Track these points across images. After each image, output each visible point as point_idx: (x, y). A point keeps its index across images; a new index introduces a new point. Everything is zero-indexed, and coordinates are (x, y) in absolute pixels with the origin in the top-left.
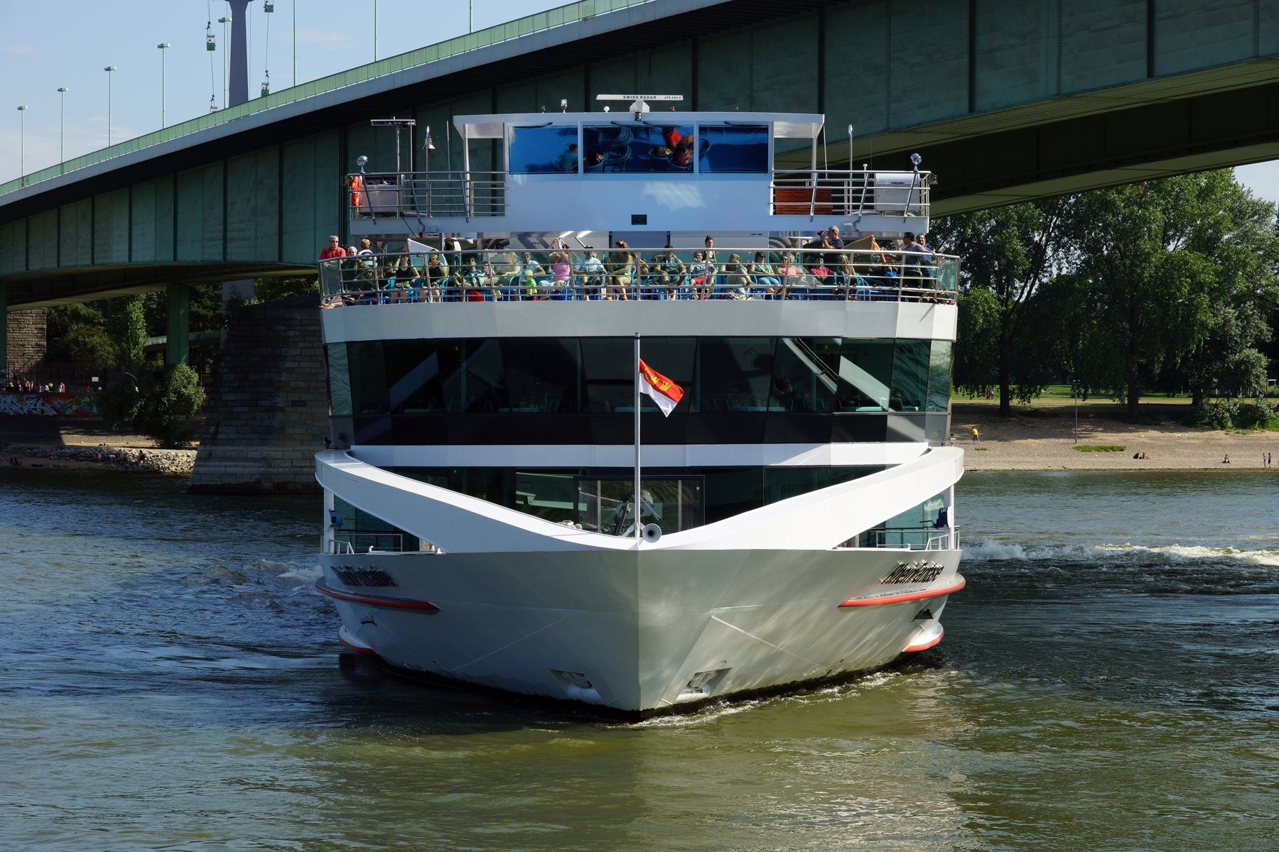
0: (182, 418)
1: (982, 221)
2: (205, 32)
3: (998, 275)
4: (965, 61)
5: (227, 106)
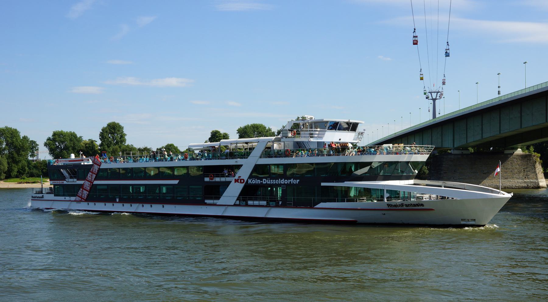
0: (424, 176)
5: (432, 119)
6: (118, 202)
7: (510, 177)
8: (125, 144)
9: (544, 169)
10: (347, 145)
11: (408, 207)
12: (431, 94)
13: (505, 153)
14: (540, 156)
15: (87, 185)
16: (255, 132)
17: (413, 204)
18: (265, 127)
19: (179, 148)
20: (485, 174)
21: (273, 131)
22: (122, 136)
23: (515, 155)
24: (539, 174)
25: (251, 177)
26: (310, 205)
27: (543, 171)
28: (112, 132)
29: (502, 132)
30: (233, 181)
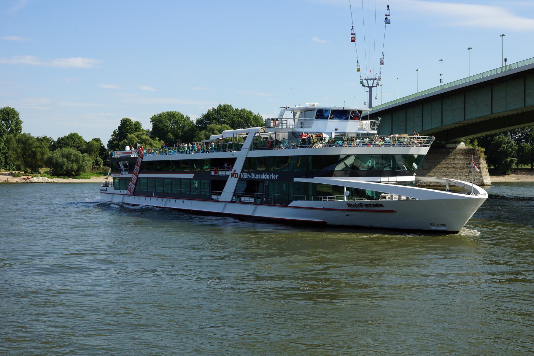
1: (527, 129)
2: (356, 64)
3: (530, 141)
4: (523, 96)
6: (153, 197)
7: (452, 173)
8: (21, 133)
9: (488, 164)
10: (322, 136)
11: (367, 207)
12: (367, 81)
13: (447, 147)
14: (484, 151)
15: (134, 178)
16: (171, 121)
17: (372, 205)
18: (183, 116)
19: (83, 138)
20: (426, 170)
21: (191, 120)
22: (18, 123)
23: (457, 150)
24: (483, 171)
25: (242, 171)
26: (284, 203)
27: (488, 167)
28: (5, 119)
29: (444, 124)
30: (230, 176)
